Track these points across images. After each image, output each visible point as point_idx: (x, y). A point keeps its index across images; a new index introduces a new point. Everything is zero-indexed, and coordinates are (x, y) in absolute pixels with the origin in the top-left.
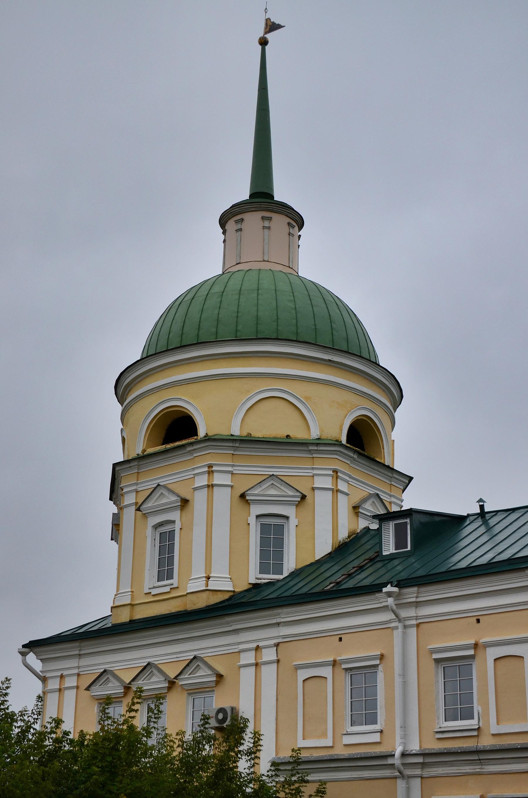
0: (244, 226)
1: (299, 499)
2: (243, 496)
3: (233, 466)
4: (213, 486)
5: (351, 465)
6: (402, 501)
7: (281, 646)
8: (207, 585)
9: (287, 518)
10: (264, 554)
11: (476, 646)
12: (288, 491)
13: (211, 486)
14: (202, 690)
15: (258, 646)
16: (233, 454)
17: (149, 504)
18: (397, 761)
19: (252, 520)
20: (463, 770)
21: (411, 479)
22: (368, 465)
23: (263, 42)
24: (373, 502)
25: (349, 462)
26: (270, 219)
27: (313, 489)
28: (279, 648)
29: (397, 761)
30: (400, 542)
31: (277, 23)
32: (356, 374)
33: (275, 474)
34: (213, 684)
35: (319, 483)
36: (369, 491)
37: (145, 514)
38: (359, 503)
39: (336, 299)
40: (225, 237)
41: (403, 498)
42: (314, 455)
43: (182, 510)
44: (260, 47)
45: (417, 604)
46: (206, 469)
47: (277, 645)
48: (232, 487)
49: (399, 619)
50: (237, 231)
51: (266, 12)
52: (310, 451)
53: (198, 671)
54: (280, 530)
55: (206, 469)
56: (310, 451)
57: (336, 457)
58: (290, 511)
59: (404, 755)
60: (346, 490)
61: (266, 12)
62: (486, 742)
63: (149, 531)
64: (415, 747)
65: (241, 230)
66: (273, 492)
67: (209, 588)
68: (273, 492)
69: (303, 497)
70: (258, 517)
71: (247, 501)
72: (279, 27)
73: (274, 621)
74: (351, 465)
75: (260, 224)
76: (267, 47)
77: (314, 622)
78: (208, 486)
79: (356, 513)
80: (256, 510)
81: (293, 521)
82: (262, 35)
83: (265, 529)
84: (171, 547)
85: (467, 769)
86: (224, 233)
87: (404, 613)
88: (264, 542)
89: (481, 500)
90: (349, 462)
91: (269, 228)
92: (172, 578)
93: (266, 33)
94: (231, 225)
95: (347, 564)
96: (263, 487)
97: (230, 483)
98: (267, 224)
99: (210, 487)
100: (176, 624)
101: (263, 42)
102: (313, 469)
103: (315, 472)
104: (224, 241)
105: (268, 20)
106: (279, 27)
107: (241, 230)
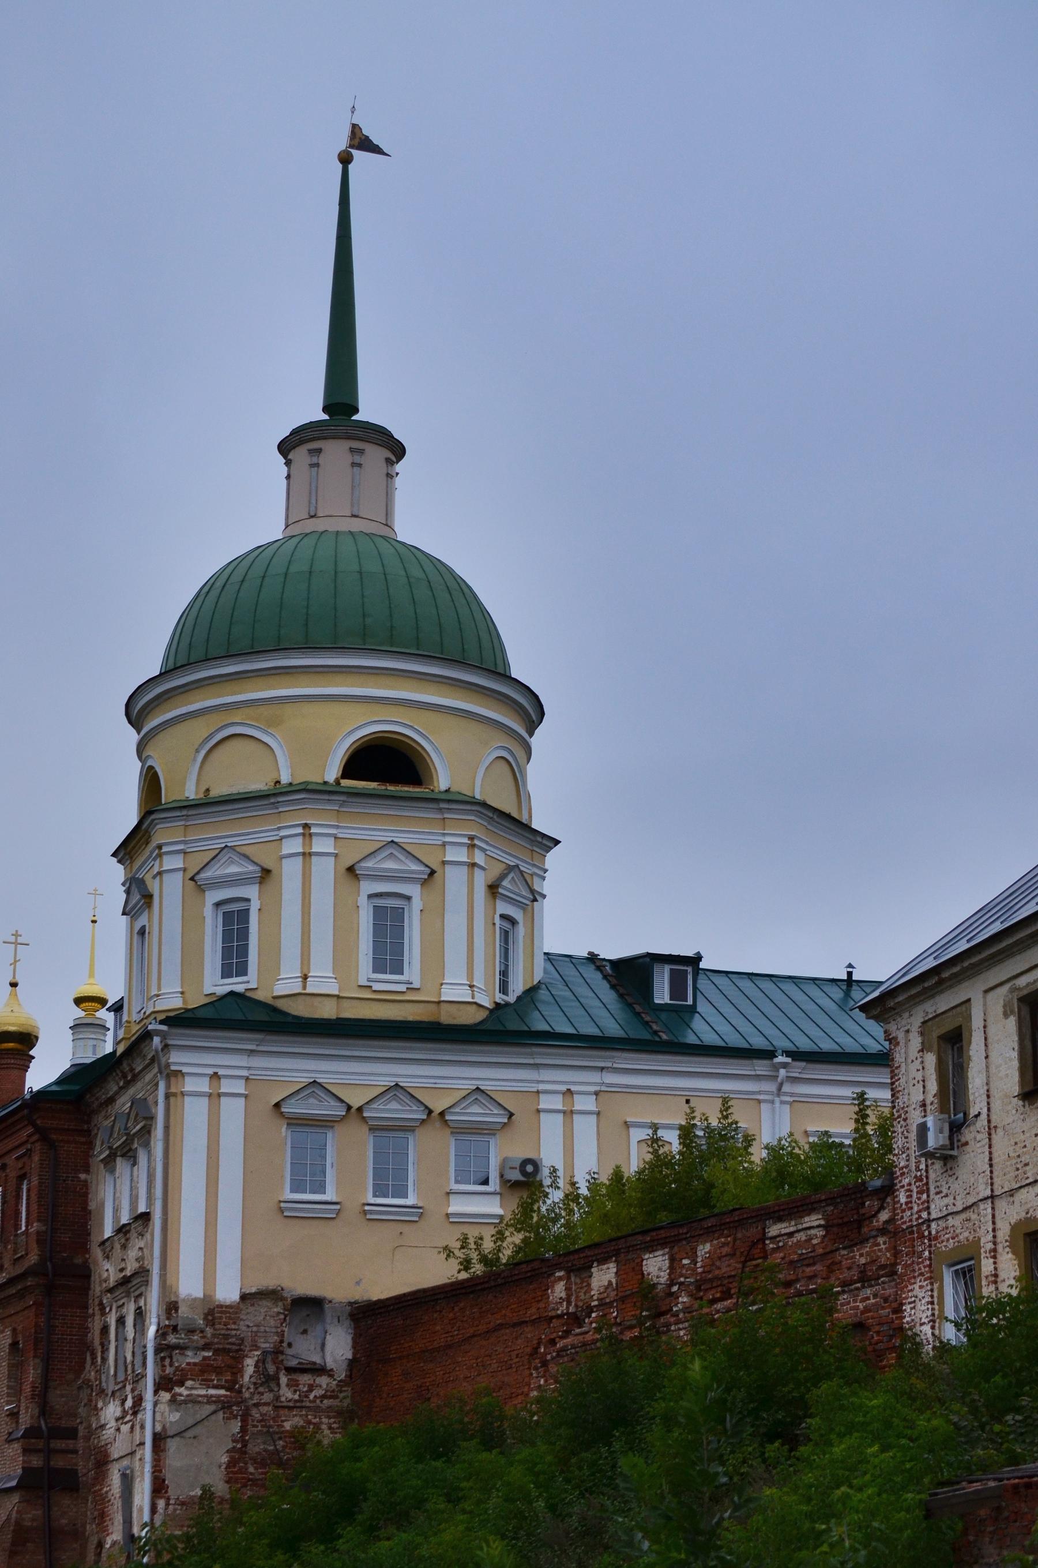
0: (322, 459)
1: (426, 877)
2: (351, 870)
3: (337, 827)
4: (310, 854)
5: (489, 827)
6: (546, 871)
7: (602, 1095)
8: (304, 988)
9: (408, 898)
10: (378, 947)
12: (410, 864)
13: (307, 855)
14: (479, 1131)
15: (109, 1029)
16: (338, 811)
17: (207, 874)
19: (363, 900)
21: (557, 842)
22: (512, 827)
23: (345, 160)
24: (513, 878)
25: (486, 824)
26: (361, 452)
27: (444, 863)
28: (599, 1097)
31: (375, 142)
32: (504, 702)
33: (396, 840)
34: (499, 1127)
35: (454, 854)
36: (507, 862)
37: (200, 885)
38: (498, 879)
39: (459, 580)
40: (289, 471)
41: (546, 867)
42: (446, 816)
43: (260, 883)
44: (340, 166)
47: (596, 1093)
48: (336, 855)
50: (312, 465)
51: (353, 112)
52: (440, 810)
53: (390, 1102)
54: (399, 915)
55: (300, 830)
56: (440, 809)
57: (473, 818)
58: (413, 890)
60: (482, 864)
61: (353, 112)
63: (208, 910)
65: (317, 465)
66: (390, 865)
67: (309, 990)
68: (390, 865)
69: (432, 873)
70: (370, 896)
71: (357, 875)
73: (531, 1061)
74: (489, 827)
75: (349, 458)
76: (350, 166)
77: (655, 1075)
78: (304, 854)
79: (493, 893)
80: (368, 887)
81: (417, 903)
82: (344, 148)
83: (379, 913)
84: (244, 934)
86: (288, 463)
88: (379, 929)
90: (486, 824)
91: (360, 465)
92: (244, 972)
93: (351, 146)
94: (300, 455)
96: (379, 858)
97: (332, 850)
98: (357, 459)
99: (307, 855)
101: (345, 160)
102: (444, 834)
103: (448, 839)
104: (288, 477)
105: (354, 126)
107: (317, 465)
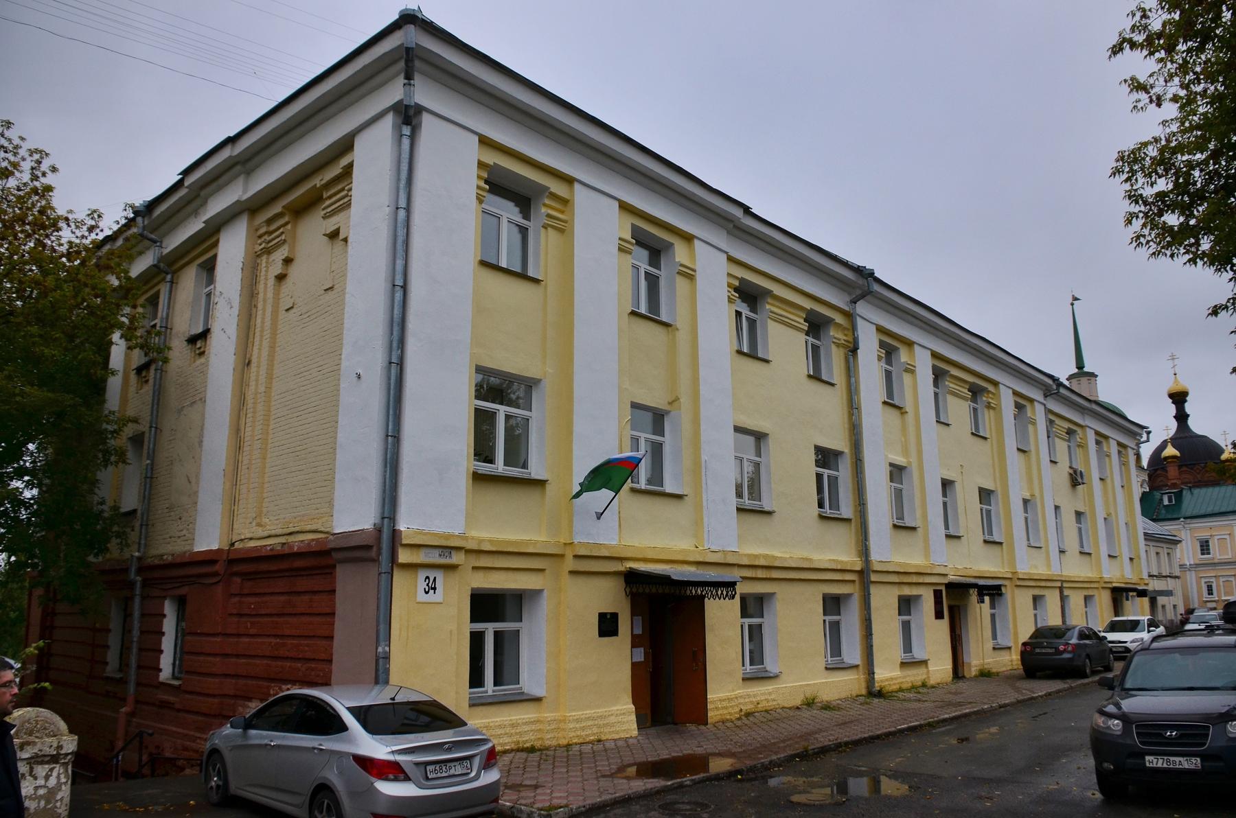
0: (1081, 382)
11: (1211, 536)
18: (1188, 566)
20: (990, 423)
23: (1072, 304)
29: (1188, 566)
30: (1170, 500)
45: (1189, 524)
46: (148, 480)
49: (1184, 527)
59: (1190, 565)
62: (1216, 561)
64: (1192, 563)
72: (1079, 299)
85: (1210, 568)
87: (1186, 526)
89: (223, 329)
95: (333, 182)
100: (986, 353)
101: (1072, 304)
106: (1079, 299)
